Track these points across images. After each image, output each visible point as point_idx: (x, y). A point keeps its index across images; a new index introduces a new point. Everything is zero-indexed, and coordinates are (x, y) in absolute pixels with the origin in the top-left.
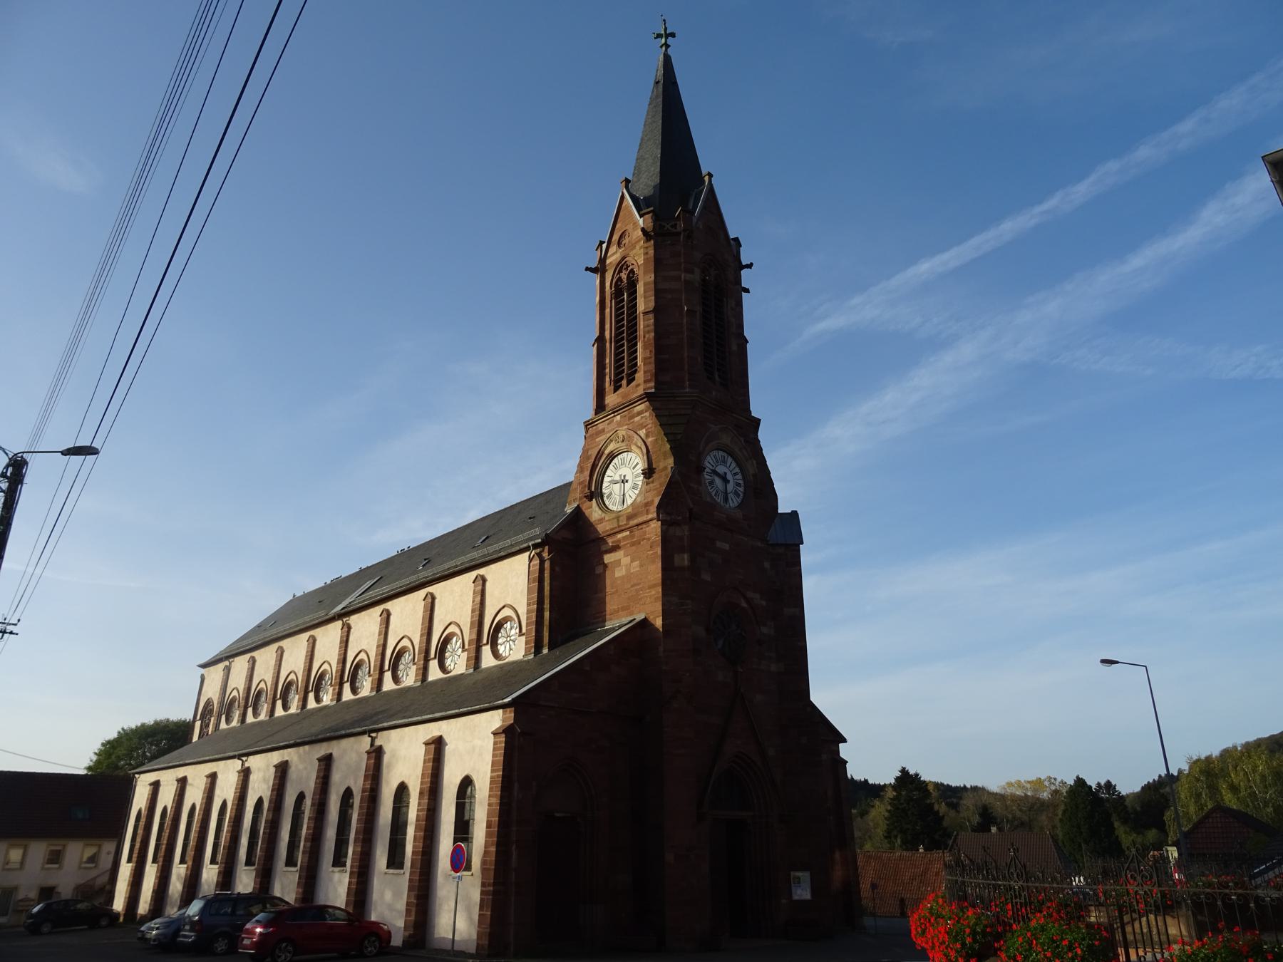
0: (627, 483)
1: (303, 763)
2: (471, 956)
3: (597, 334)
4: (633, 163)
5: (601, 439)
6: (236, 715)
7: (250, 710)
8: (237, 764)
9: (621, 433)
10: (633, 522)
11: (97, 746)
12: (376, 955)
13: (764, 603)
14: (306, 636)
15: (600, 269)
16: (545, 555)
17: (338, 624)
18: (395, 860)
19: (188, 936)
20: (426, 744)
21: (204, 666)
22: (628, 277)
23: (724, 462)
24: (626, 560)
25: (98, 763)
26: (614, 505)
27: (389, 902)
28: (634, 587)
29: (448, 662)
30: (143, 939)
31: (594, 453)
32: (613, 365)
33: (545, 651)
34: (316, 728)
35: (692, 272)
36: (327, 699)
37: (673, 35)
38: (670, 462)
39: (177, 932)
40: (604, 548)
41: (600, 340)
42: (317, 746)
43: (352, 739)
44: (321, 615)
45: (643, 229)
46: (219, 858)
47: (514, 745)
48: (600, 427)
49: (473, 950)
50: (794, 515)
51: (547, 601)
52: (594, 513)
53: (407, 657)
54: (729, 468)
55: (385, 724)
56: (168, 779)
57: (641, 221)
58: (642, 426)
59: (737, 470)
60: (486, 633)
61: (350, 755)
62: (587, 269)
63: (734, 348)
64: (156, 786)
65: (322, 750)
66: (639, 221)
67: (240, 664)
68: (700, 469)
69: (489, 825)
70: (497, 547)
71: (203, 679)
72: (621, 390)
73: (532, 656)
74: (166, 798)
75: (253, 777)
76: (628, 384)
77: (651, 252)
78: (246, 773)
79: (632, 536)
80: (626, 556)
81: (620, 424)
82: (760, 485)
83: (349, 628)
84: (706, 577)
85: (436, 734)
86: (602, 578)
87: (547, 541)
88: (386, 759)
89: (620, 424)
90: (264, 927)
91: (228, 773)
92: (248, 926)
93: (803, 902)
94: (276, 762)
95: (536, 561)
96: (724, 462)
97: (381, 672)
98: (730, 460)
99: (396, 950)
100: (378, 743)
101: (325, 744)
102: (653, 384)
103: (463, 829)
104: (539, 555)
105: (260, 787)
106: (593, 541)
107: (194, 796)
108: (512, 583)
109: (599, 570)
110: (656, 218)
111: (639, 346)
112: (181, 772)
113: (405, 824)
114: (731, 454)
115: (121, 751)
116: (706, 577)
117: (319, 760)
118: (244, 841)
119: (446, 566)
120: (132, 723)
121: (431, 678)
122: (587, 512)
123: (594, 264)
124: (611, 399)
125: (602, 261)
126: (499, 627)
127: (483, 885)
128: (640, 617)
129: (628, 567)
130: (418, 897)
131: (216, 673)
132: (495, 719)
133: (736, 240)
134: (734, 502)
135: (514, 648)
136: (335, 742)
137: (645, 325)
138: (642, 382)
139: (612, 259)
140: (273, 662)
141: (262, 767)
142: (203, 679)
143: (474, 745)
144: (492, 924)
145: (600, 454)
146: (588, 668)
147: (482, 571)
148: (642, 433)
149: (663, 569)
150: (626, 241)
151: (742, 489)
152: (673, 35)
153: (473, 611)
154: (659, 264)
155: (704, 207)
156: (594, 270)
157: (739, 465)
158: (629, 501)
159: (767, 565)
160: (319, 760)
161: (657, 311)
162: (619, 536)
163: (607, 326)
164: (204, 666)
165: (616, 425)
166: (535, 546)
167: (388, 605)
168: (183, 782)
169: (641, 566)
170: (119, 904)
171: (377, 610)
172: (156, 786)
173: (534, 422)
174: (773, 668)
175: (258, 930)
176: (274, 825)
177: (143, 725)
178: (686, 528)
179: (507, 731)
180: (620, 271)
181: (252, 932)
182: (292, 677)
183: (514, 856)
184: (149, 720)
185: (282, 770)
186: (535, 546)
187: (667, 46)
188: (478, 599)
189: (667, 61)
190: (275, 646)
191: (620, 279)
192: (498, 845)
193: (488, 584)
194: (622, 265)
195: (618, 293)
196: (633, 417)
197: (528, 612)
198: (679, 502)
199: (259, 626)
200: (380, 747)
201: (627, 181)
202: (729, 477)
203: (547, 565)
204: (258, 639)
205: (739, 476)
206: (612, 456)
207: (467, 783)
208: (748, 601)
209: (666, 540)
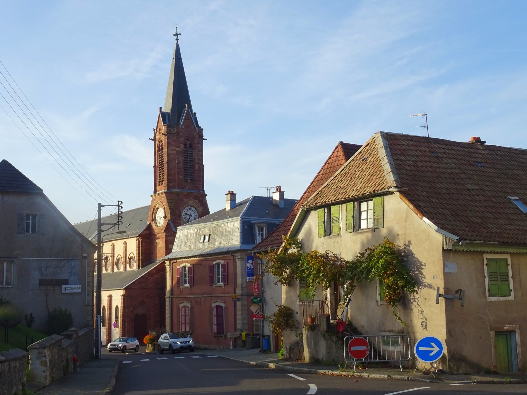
3: (154, 164)
5: (155, 202)
15: (154, 139)
23: (190, 210)
35: (179, 147)
37: (180, 34)
38: (170, 215)
47: (126, 299)
52: (154, 226)
63: (197, 168)
68: (180, 216)
87: (139, 236)
96: (190, 210)
98: (193, 208)
103: (117, 317)
110: (169, 127)
114: (193, 206)
123: (153, 138)
125: (155, 137)
132: (121, 292)
135: (135, 267)
137: (165, 166)
145: (155, 207)
152: (180, 34)
154: (169, 144)
156: (153, 140)
157: (196, 209)
161: (168, 162)
179: (124, 296)
187: (177, 40)
195: (159, 150)
201: (161, 108)
202: (193, 214)
206: (158, 209)
207: (117, 307)
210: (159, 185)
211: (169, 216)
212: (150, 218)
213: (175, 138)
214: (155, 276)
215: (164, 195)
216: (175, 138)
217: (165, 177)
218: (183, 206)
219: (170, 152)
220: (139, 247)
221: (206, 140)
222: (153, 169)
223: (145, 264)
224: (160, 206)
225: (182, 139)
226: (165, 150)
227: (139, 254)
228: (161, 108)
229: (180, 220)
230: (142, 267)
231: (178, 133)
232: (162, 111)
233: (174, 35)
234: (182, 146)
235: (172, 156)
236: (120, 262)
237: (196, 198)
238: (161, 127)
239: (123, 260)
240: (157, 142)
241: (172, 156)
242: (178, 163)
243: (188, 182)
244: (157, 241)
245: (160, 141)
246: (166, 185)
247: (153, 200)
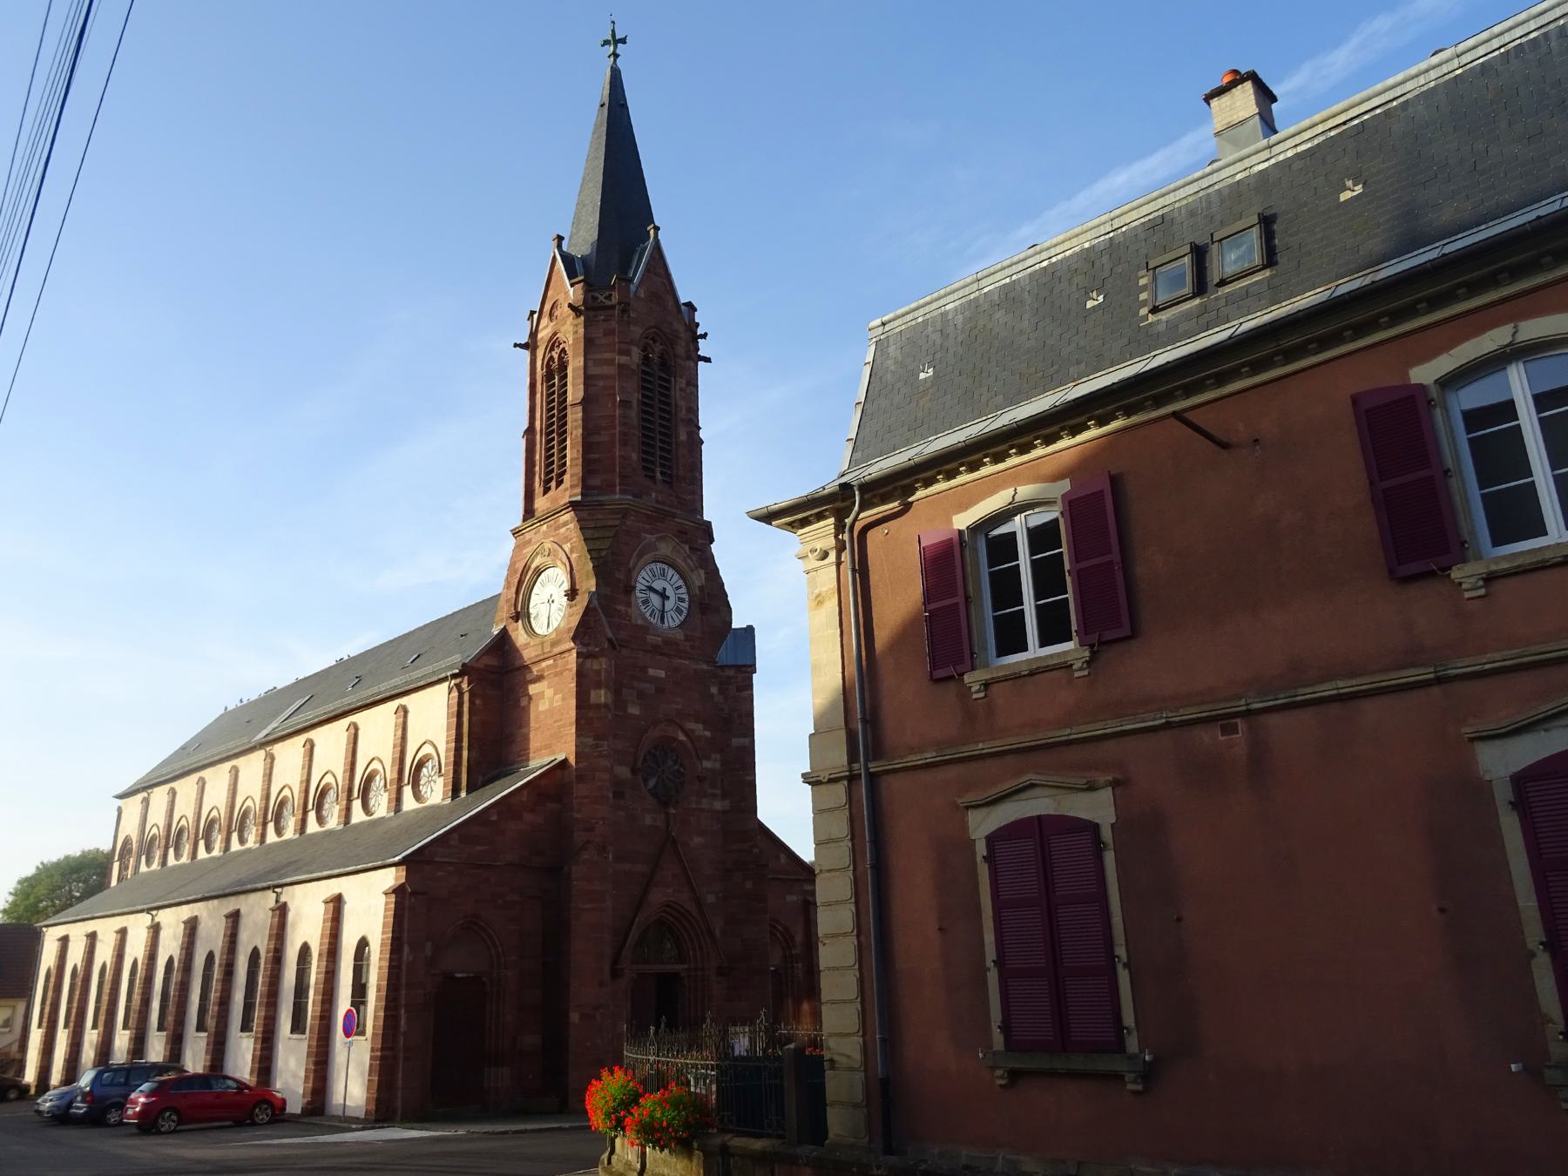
0: (552, 608)
1: (211, 918)
3: (526, 425)
4: (574, 208)
5: (529, 550)
6: (187, 849)
7: (171, 851)
8: (146, 919)
9: (548, 545)
10: (557, 650)
11: (11, 884)
12: (268, 1123)
13: (708, 734)
14: (227, 766)
15: (530, 345)
16: (465, 686)
17: (261, 754)
18: (298, 1026)
19: (80, 1108)
20: (326, 902)
21: (121, 797)
24: (549, 693)
25: (14, 904)
26: (540, 627)
27: (291, 1074)
28: (552, 728)
29: (372, 802)
30: (39, 1112)
31: (520, 566)
32: (541, 468)
33: (463, 794)
34: (215, 885)
35: (628, 353)
36: (252, 841)
37: (623, 41)
39: (70, 1105)
40: (529, 677)
41: (530, 432)
42: (224, 901)
43: (259, 894)
44: (243, 742)
45: (570, 306)
46: (131, 1023)
48: (528, 536)
49: (362, 1115)
50: (750, 630)
51: (465, 739)
52: (519, 636)
53: (331, 795)
54: (671, 583)
55: (288, 880)
56: (77, 934)
57: (571, 290)
58: (567, 539)
59: (681, 583)
60: (409, 774)
61: (256, 910)
63: (683, 437)
64: (65, 940)
65: (230, 905)
66: (571, 293)
67: (159, 796)
68: (630, 589)
69: (378, 990)
70: (429, 669)
71: (120, 810)
72: (550, 493)
74: (75, 956)
75: (163, 934)
77: (581, 331)
78: (155, 929)
79: (555, 666)
80: (549, 687)
81: (546, 535)
82: (710, 598)
83: (273, 759)
84: (634, 710)
85: (337, 891)
86: (526, 710)
87: (465, 670)
88: (291, 916)
89: (546, 535)
90: (147, 1097)
91: (137, 927)
92: (133, 1096)
93: (750, 1058)
94: (185, 918)
95: (455, 694)
97: (305, 812)
98: (671, 572)
99: (293, 1119)
100: (283, 899)
101: (232, 899)
102: (579, 490)
103: (359, 990)
104: (458, 686)
105: (170, 946)
106: (519, 669)
107: (104, 954)
108: (432, 716)
109: (524, 702)
110: (589, 287)
112: (90, 926)
113: (308, 987)
115: (42, 890)
116: (634, 710)
117: (227, 917)
118: (156, 1005)
119: (375, 690)
120: (54, 855)
122: (513, 635)
123: (524, 339)
124: (541, 503)
125: (533, 335)
126: (420, 765)
127: (373, 1050)
128: (561, 757)
130: (316, 1063)
131: (133, 806)
132: (389, 878)
134: (673, 620)
135: (436, 791)
136: (242, 897)
137: (575, 417)
138: (568, 490)
139: (544, 335)
140: (194, 796)
141: (172, 921)
142: (120, 810)
143: (369, 903)
144: (379, 1090)
145: (526, 569)
146: (494, 818)
147: (403, 701)
148: (567, 547)
149: (578, 707)
150: (557, 313)
151: (686, 605)
152: (623, 41)
154: (589, 343)
155: (647, 270)
156: (524, 346)
157: (682, 576)
158: (554, 624)
159: (714, 690)
160: (227, 917)
161: (586, 402)
162: (544, 664)
163: (538, 415)
164: (121, 797)
165: (541, 534)
166: (454, 676)
167: (312, 734)
168: (92, 937)
169: (564, 699)
170: (30, 1076)
171: (300, 740)
172: (65, 940)
173: (458, 525)
174: (718, 805)
175: (142, 1100)
176: (184, 987)
177: (67, 858)
178: (603, 660)
179: (398, 891)
180: (552, 349)
181: (135, 1103)
182: (214, 813)
183: (403, 1022)
184: (75, 851)
185: (192, 926)
186: (454, 676)
187: (616, 56)
188: (399, 733)
189: (616, 77)
190: (195, 777)
191: (552, 358)
192: (386, 1009)
193: (410, 716)
194: (553, 343)
195: (549, 376)
196: (558, 528)
197: (447, 750)
198: (602, 625)
199: (183, 748)
200: (285, 904)
201: (560, 239)
202: (669, 592)
203: (466, 697)
204: (178, 767)
205: (683, 590)
206: (538, 572)
207: (363, 944)
208: (686, 734)
209: (581, 675)
210: (546, 490)
211: (589, 584)
212: (504, 611)
213: (613, 324)
214: (527, 816)
215: (568, 516)
216: (613, 324)
217: (573, 453)
218: (640, 556)
219: (594, 371)
220: (459, 715)
221: (708, 360)
222: (523, 443)
223: (480, 779)
224: (549, 561)
225: (637, 331)
226: (575, 364)
227: (458, 739)
228: (560, 239)
229: (629, 604)
230: (468, 792)
231: (625, 307)
232: (565, 248)
233: (606, 43)
234: (636, 353)
235: (601, 383)
236: (378, 782)
237: (682, 534)
238: (561, 297)
239: (391, 774)
240: (540, 353)
241: (601, 383)
242: (625, 404)
243: (653, 478)
244: (533, 689)
245: (553, 343)
246: (577, 480)
247: (518, 548)
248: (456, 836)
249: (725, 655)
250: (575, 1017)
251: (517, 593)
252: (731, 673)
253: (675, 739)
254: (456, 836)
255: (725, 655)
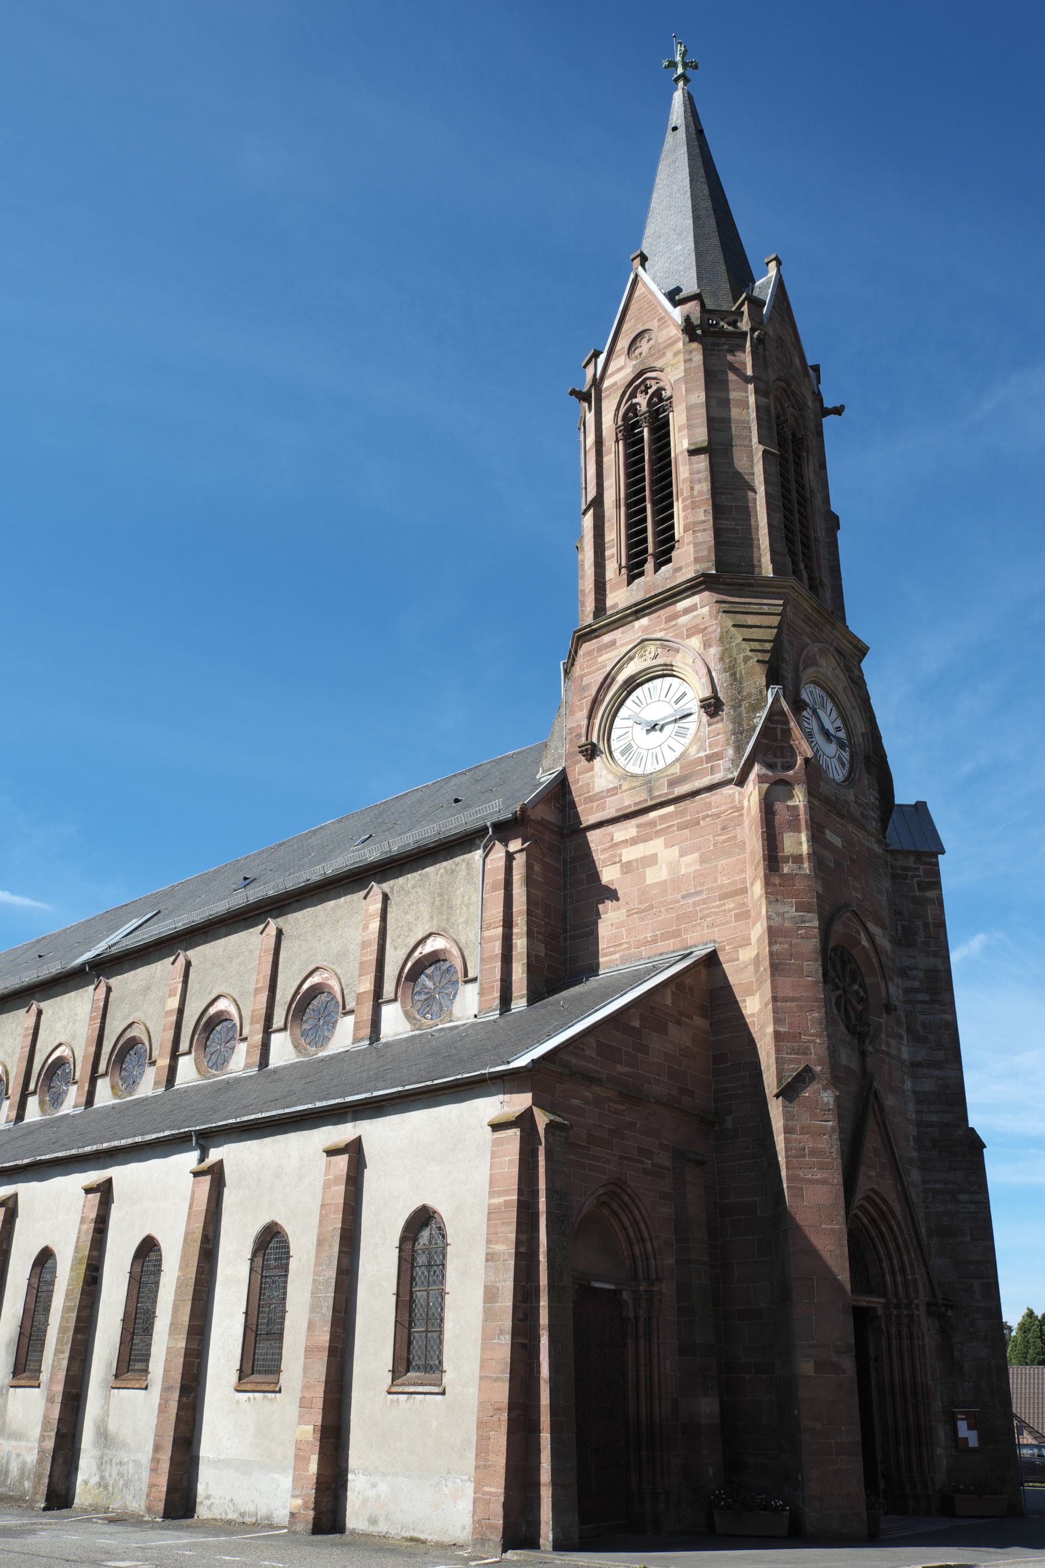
2: (447, 1549)
10: (679, 791)
22: (650, 403)
50: (921, 807)
62: (573, 392)
73: (366, 1043)
76: (656, 571)
80: (667, 846)
98: (830, 705)
111: (678, 509)
114: (832, 696)
121: (27, 1120)
129: (673, 867)
133: (816, 368)
146: (636, 1024)
150: (644, 347)
153: (92, 1019)
156: (585, 397)
169: (703, 860)
180: (633, 395)
191: (633, 408)
194: (638, 382)
195: (629, 430)
206: (632, 685)
207: (45, 1258)
208: (871, 938)
230: (534, 996)
248: (592, 1041)
249: (897, 836)
250: (806, 1367)
251: (590, 716)
252: (910, 862)
253: (859, 942)
254: (592, 1041)
255: (897, 836)
